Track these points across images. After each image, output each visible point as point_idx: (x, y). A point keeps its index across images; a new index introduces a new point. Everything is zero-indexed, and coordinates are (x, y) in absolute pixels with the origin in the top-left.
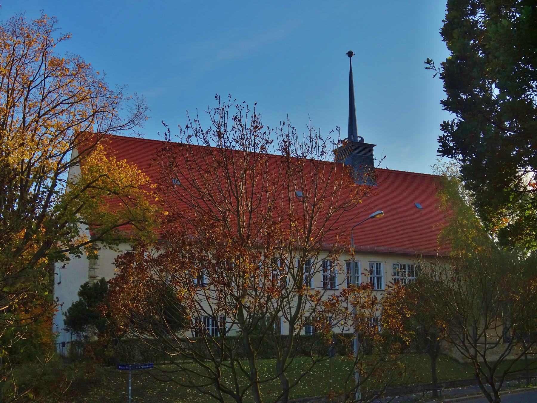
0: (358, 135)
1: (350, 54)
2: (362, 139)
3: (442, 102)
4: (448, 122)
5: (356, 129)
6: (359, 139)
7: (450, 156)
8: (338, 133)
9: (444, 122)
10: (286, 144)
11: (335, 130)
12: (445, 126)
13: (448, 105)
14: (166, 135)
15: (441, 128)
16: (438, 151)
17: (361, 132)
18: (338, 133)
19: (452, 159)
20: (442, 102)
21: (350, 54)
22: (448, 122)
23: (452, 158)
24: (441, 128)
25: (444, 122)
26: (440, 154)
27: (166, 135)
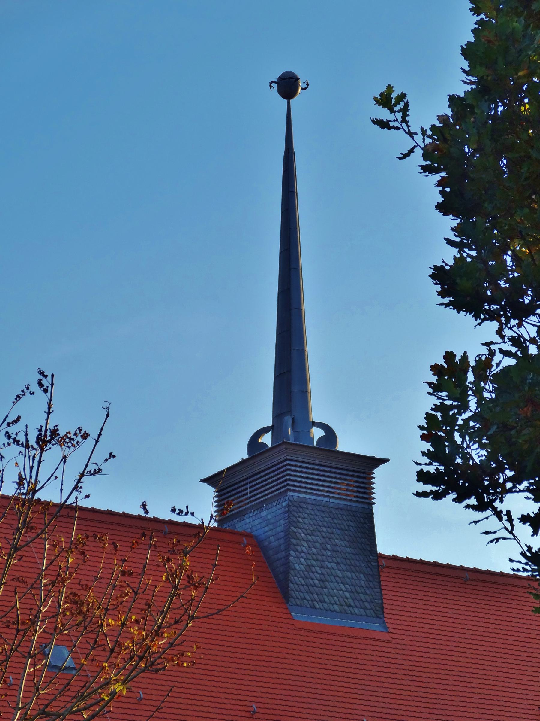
0: (316, 416)
1: (288, 86)
2: (330, 435)
3: (430, 276)
4: (465, 356)
5: (305, 392)
6: (317, 433)
7: (473, 501)
8: (45, 398)
9: (449, 356)
10: (533, 513)
11: (34, 387)
12: (450, 374)
13: (459, 288)
14: (497, 540)
15: (434, 379)
16: (423, 477)
17: (321, 408)
18: (45, 398)
19: (479, 515)
20: (430, 276)
21: (288, 86)
22: (465, 356)
23: (481, 507)
24: (434, 379)
25: (449, 356)
26: (429, 488)
27: (497, 540)
